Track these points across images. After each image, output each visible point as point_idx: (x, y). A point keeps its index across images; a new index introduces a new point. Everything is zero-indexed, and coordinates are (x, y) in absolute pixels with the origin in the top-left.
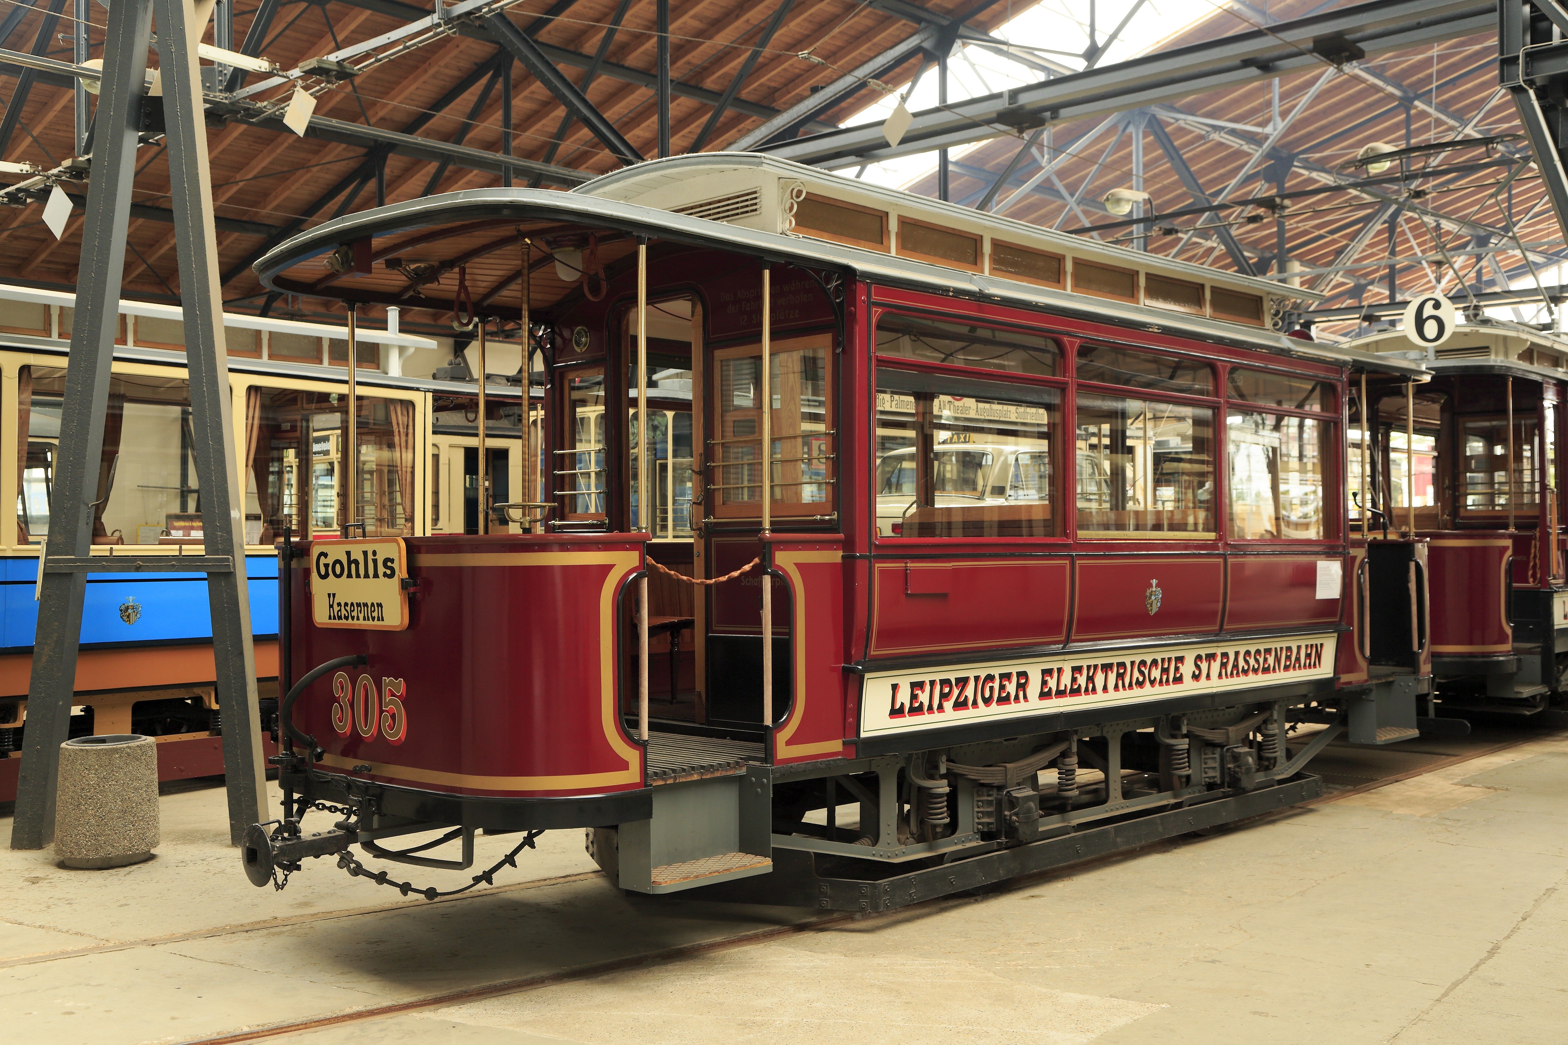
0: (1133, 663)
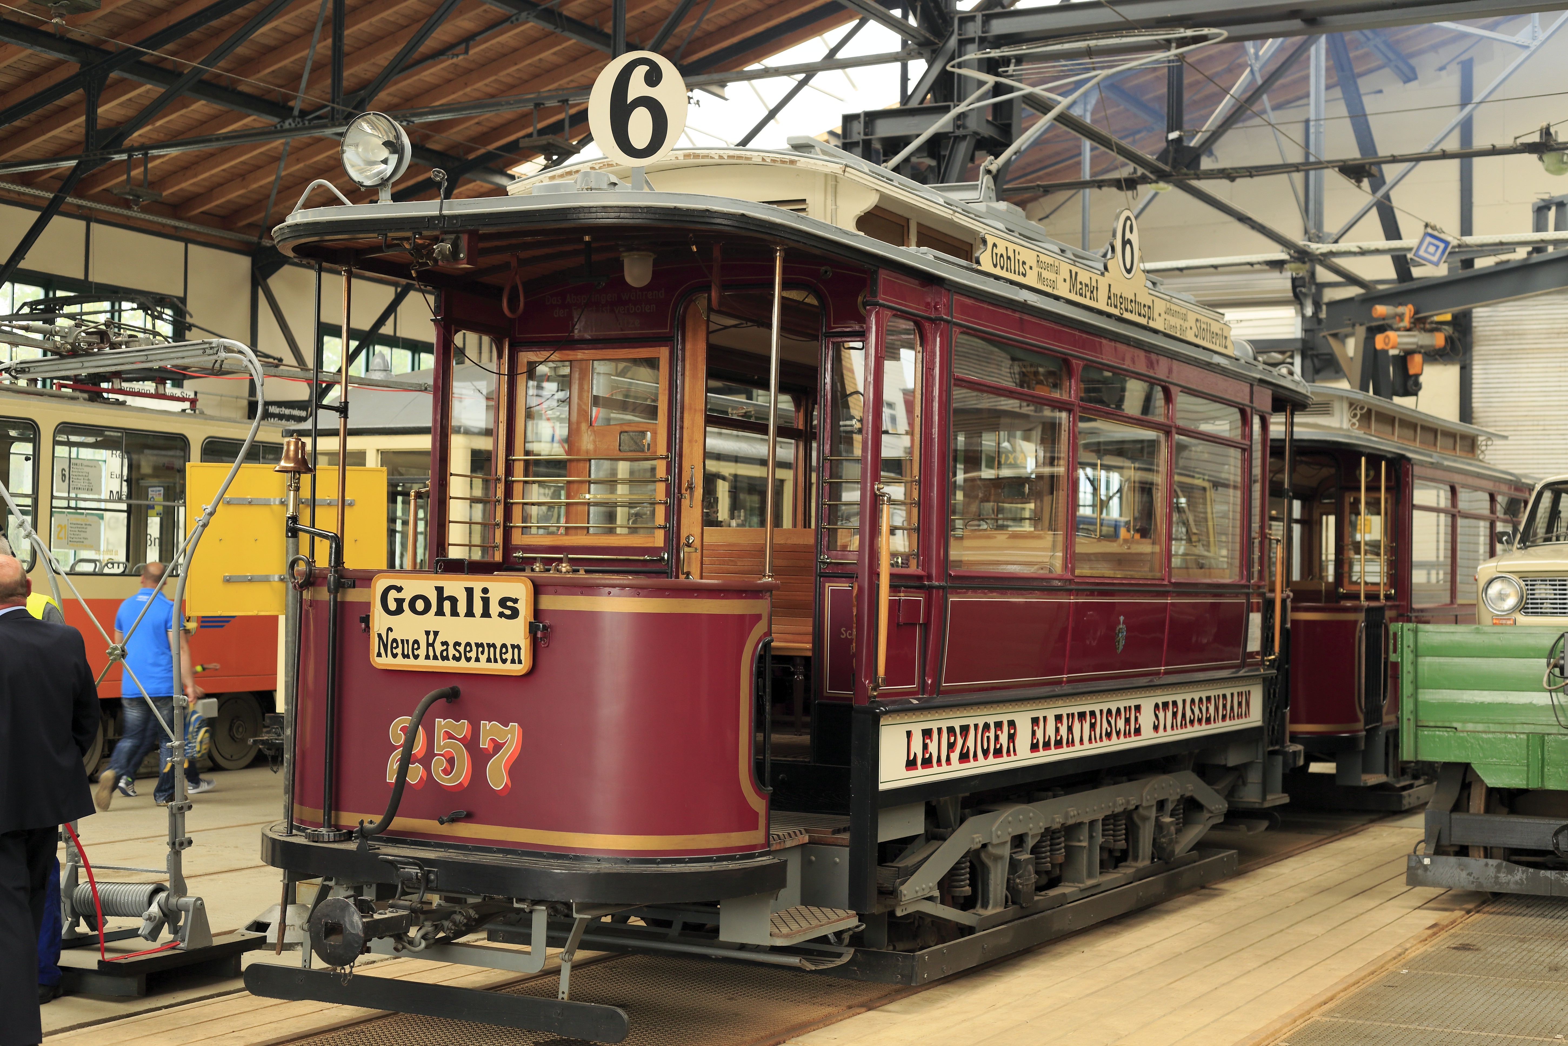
0: (1101, 711)
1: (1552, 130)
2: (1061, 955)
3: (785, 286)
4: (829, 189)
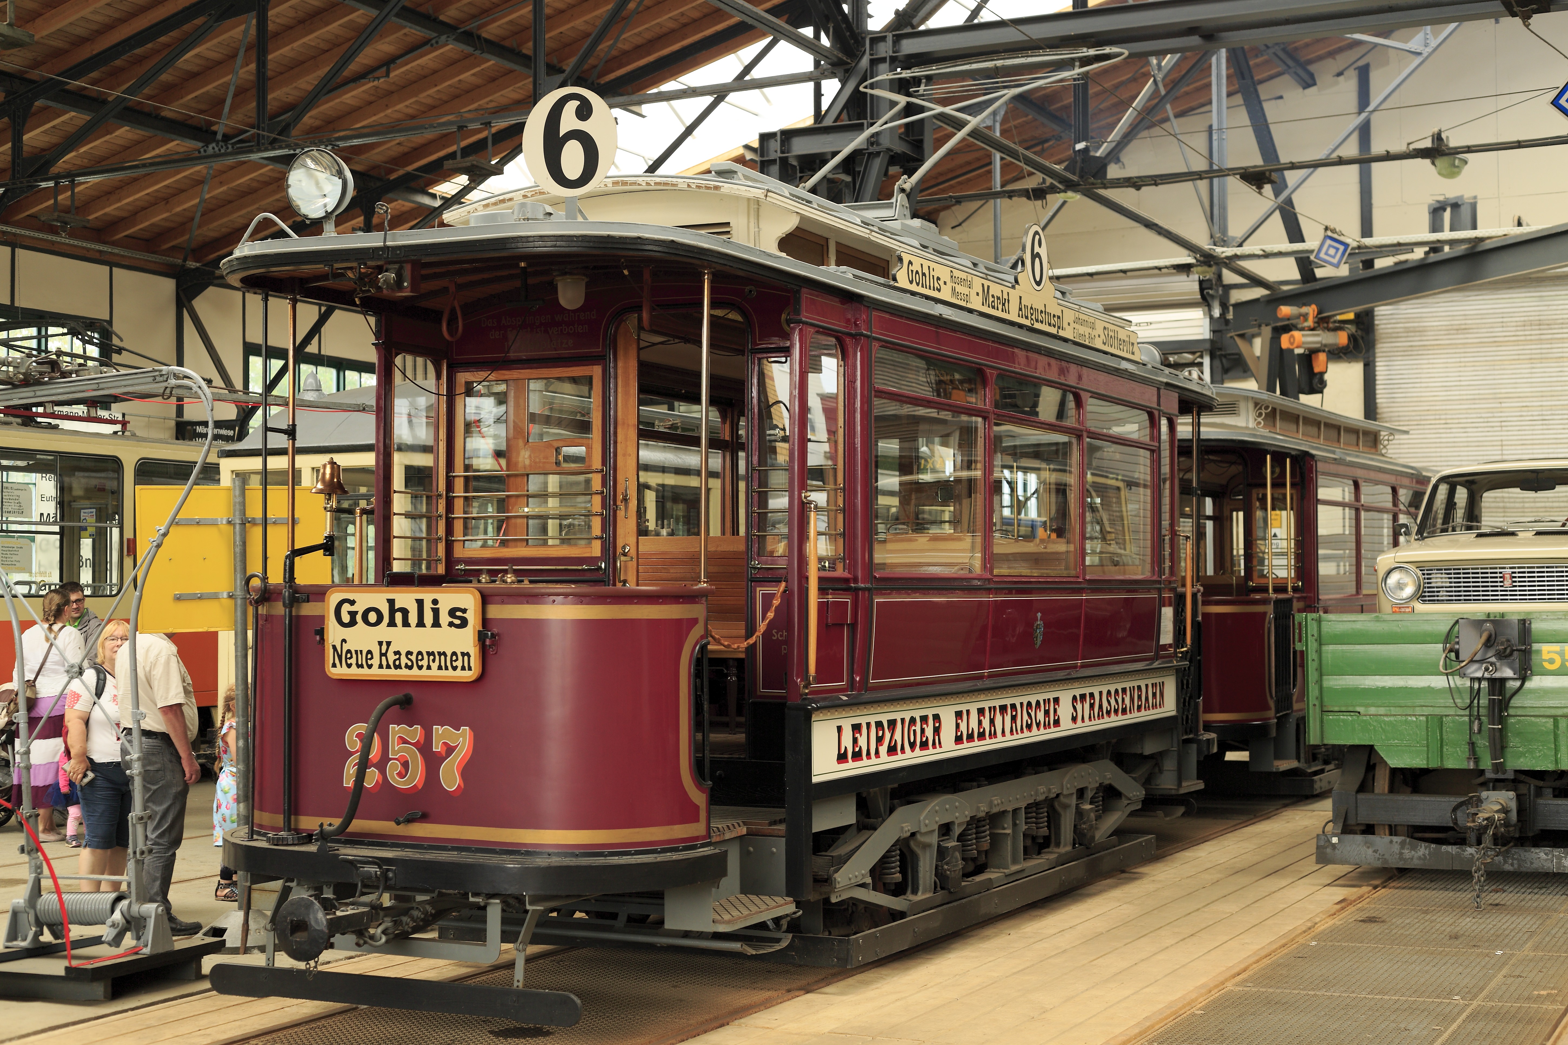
0: (1022, 704)
1: (1444, 136)
2: (988, 938)
3: (713, 305)
4: (752, 212)
